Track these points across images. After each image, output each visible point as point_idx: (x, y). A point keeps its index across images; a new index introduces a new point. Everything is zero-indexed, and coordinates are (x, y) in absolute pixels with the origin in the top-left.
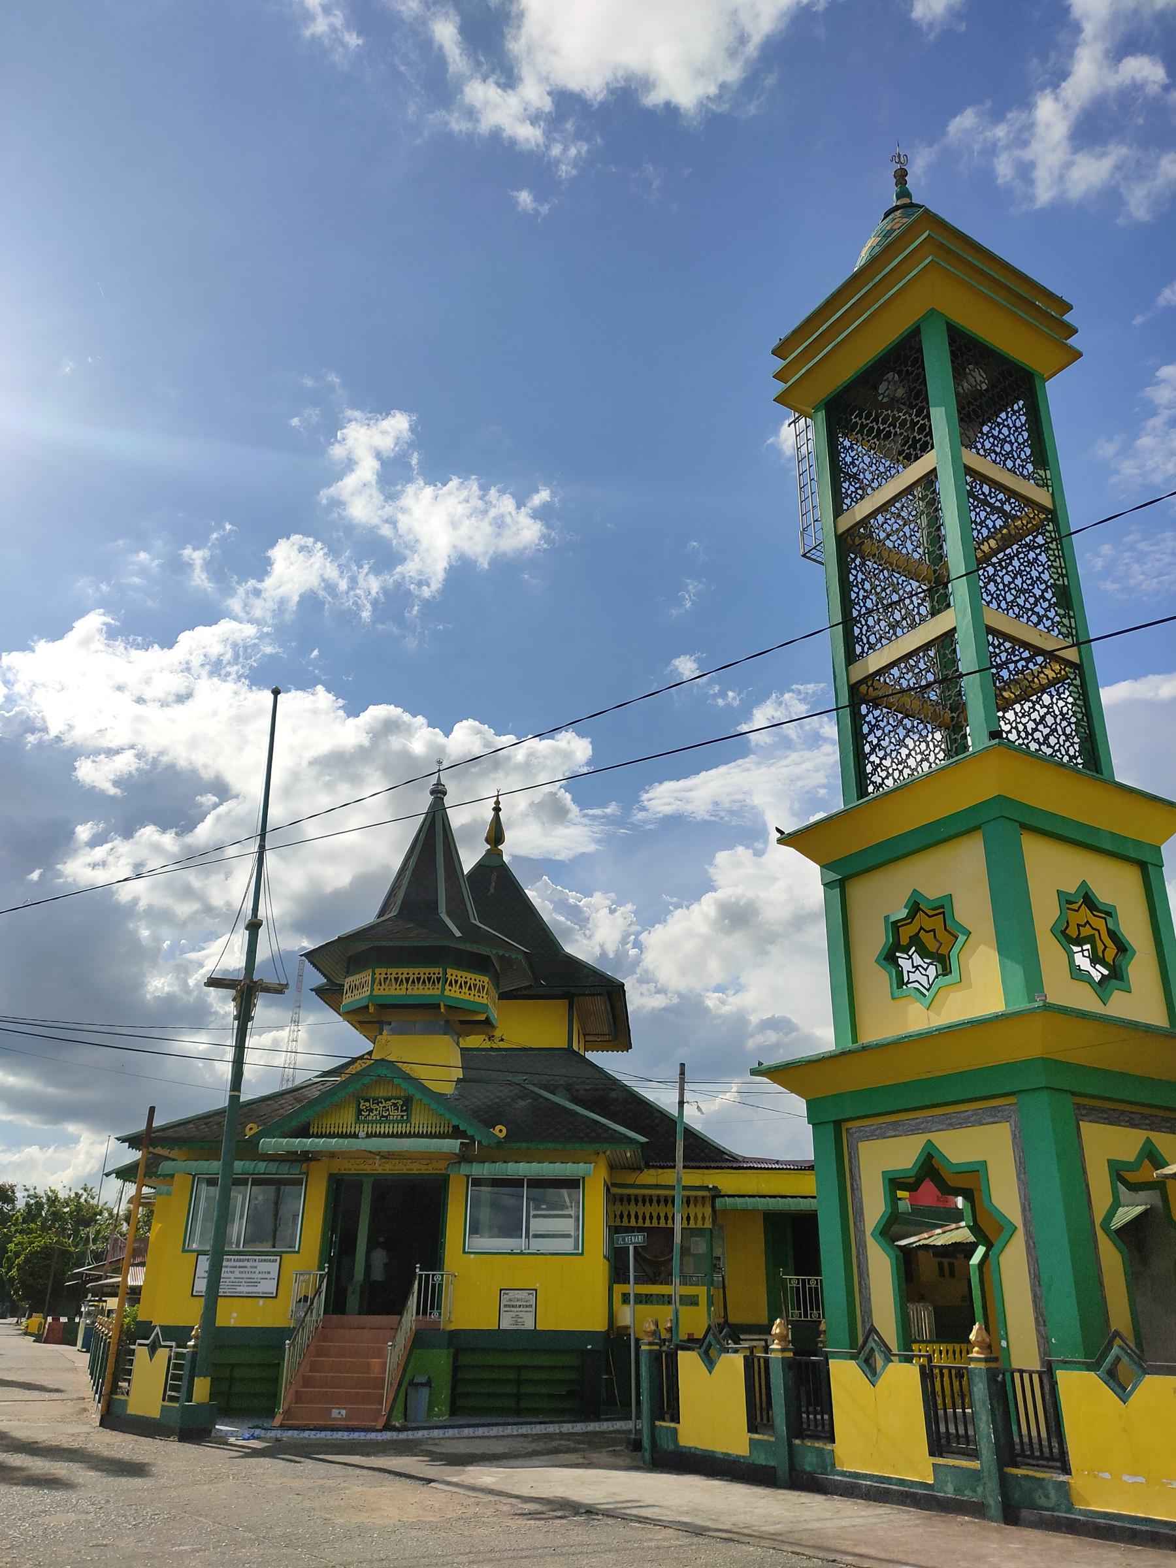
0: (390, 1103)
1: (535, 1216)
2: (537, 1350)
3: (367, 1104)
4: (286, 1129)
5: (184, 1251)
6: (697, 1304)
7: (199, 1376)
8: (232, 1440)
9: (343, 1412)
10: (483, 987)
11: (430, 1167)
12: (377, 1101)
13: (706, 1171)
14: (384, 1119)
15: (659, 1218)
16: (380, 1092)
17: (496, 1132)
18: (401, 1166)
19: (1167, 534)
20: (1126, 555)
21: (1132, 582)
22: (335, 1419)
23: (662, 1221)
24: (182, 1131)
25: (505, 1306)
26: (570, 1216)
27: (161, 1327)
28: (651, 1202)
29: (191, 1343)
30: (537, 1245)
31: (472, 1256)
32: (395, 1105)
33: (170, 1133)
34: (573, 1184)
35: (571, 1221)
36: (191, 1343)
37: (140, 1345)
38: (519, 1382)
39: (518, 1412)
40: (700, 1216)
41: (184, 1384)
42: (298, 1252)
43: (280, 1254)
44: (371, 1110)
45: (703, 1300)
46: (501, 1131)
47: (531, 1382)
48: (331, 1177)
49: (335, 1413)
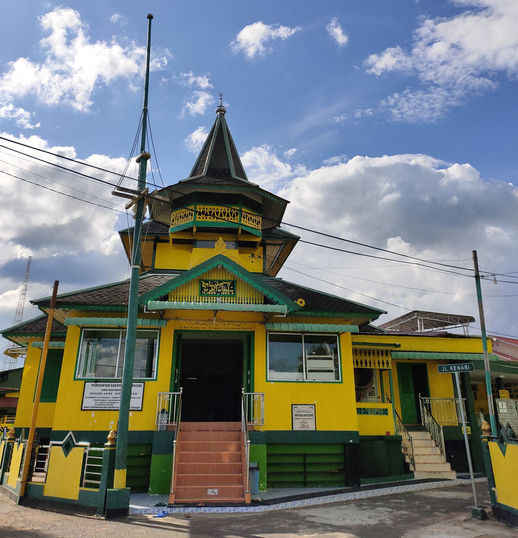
0: (222, 284)
1: (309, 359)
2: (298, 444)
3: (207, 284)
4: (157, 297)
5: (75, 379)
6: (387, 414)
7: (119, 468)
8: (150, 517)
9: (216, 491)
10: (259, 222)
11: (240, 327)
12: (213, 282)
13: (381, 337)
14: (219, 294)
15: (361, 363)
16: (215, 277)
17: (298, 302)
18: (221, 326)
19: (420, 91)
20: (403, 98)
21: (404, 111)
22: (211, 496)
23: (364, 365)
24: (75, 299)
25: (296, 415)
26: (331, 359)
27: (74, 432)
28: (374, 354)
29: (109, 443)
30: (312, 376)
31: (272, 383)
32: (225, 285)
33: (67, 299)
34: (332, 339)
35: (332, 362)
36: (109, 443)
37: (54, 445)
38: (305, 464)
39: (305, 484)
40: (377, 362)
41: (103, 474)
42: (156, 380)
43: (143, 382)
44: (210, 288)
45: (390, 411)
46: (301, 302)
47: (311, 464)
48: (176, 331)
49: (210, 492)
